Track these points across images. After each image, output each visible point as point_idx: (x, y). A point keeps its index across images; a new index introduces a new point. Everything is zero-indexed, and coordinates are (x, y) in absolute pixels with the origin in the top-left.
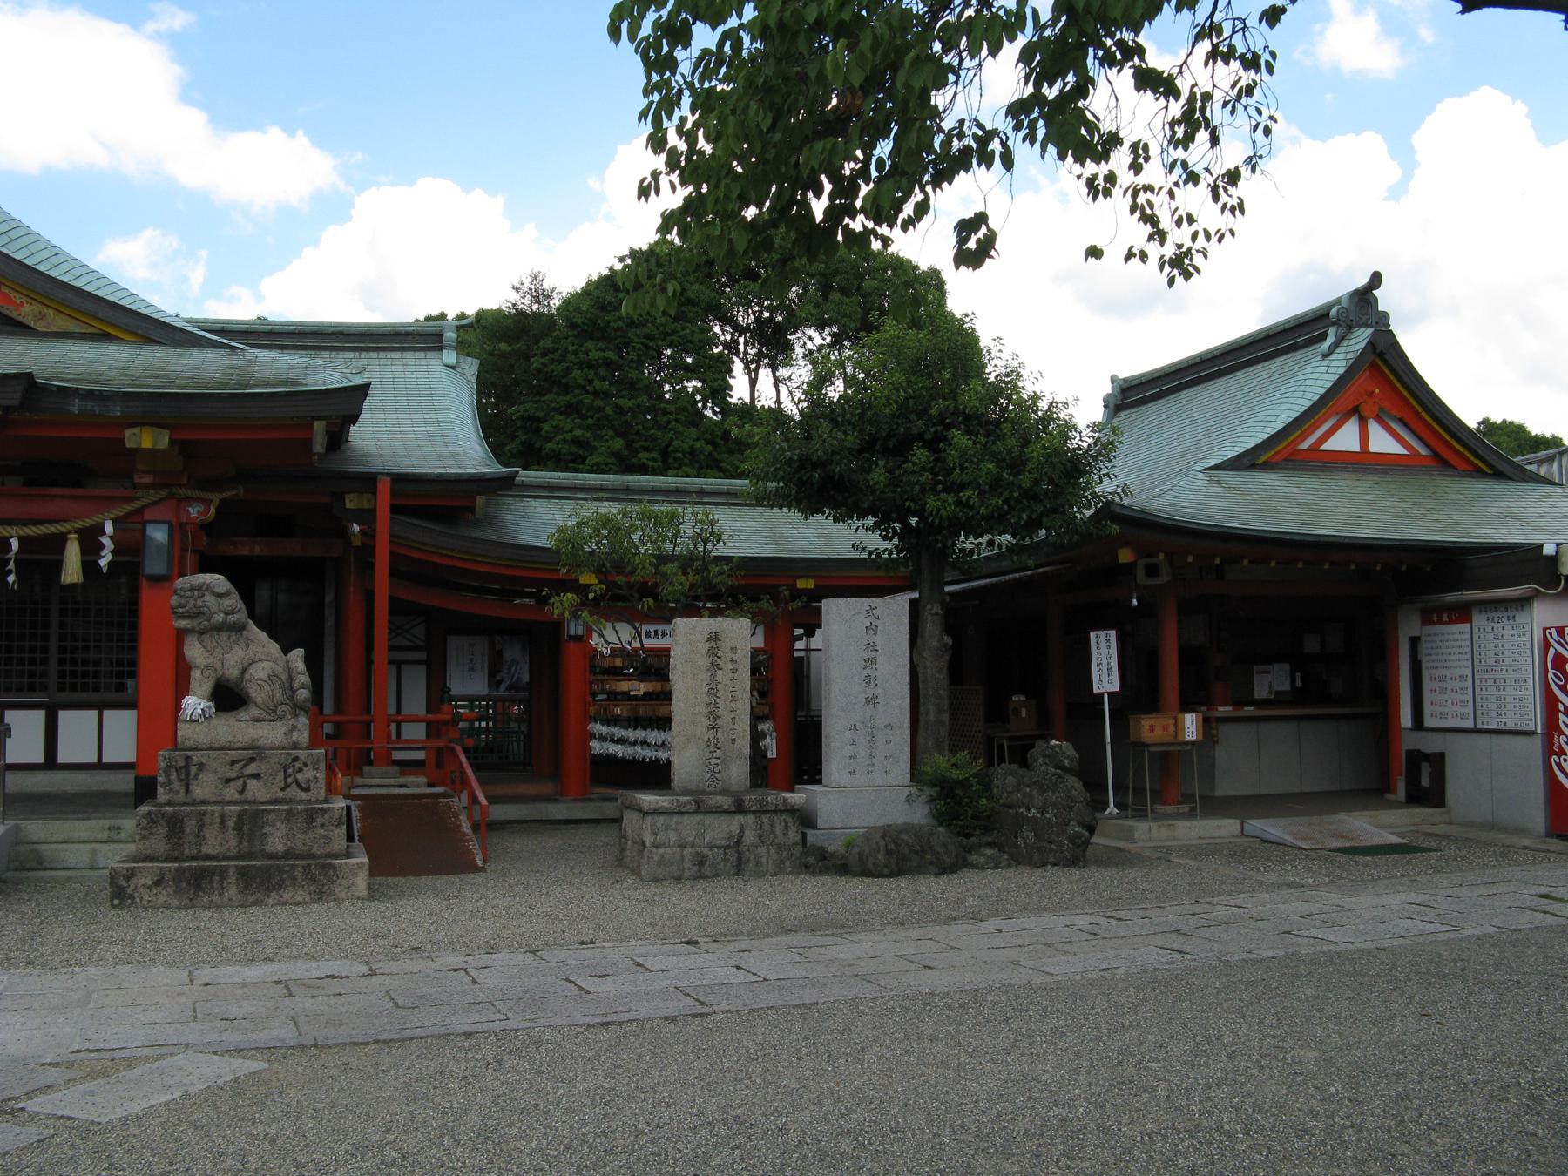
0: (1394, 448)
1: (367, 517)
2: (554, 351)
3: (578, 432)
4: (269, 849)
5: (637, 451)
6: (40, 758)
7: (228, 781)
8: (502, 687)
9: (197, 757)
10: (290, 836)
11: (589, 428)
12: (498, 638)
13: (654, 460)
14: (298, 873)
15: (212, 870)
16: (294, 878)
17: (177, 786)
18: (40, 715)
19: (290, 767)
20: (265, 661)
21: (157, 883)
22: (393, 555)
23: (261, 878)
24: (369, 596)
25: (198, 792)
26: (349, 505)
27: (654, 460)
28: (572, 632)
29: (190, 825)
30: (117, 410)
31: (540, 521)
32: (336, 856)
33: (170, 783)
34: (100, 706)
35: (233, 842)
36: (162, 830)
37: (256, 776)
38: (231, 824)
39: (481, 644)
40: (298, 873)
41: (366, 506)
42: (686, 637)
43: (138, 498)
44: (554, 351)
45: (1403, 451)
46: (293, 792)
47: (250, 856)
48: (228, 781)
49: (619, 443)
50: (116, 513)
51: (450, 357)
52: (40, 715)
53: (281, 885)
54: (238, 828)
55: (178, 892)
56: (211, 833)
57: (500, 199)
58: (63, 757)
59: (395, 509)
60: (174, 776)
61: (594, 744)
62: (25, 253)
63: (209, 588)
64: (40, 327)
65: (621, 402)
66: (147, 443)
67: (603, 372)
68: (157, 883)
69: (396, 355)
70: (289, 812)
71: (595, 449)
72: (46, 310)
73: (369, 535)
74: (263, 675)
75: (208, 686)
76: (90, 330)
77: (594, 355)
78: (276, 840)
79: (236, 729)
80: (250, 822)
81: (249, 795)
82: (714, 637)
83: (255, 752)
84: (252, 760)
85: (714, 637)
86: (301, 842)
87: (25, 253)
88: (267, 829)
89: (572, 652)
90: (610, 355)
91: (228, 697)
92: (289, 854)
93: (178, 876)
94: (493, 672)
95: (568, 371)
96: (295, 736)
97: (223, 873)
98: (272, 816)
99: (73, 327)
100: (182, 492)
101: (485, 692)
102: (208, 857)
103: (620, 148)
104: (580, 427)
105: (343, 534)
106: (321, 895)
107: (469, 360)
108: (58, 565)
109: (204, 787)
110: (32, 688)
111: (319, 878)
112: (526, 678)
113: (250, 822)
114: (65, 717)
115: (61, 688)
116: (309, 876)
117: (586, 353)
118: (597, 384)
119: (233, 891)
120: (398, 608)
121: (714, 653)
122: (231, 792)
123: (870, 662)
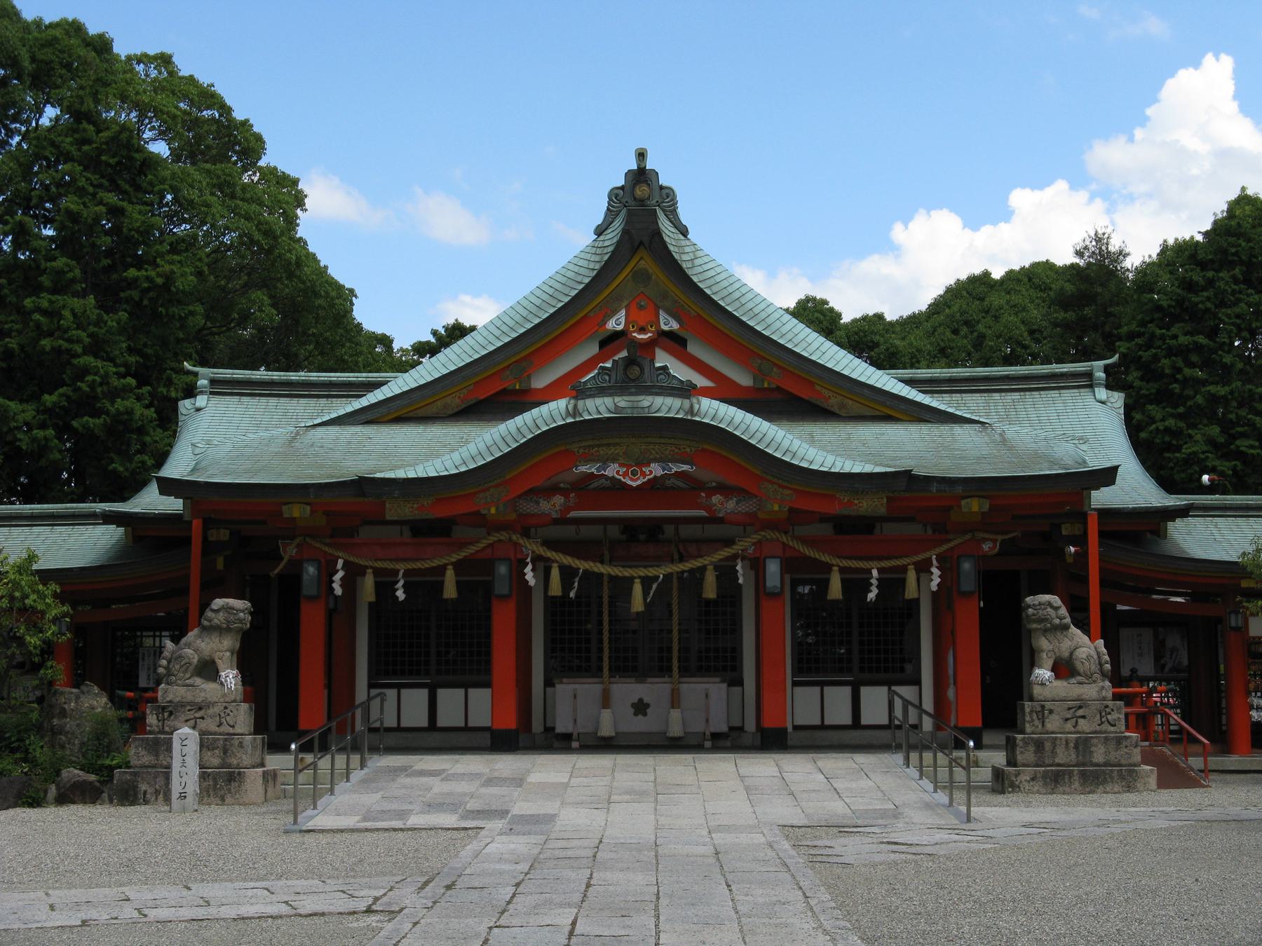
1: (1081, 540)
2: (1139, 335)
3: (1171, 422)
4: (1095, 760)
5: (1234, 437)
7: (1067, 720)
8: (1167, 669)
9: (1048, 705)
10: (1107, 753)
11: (1180, 417)
12: (1161, 629)
13: (1252, 447)
14: (1115, 774)
15: (1064, 772)
16: (1112, 778)
17: (1037, 722)
19: (1104, 711)
20: (1087, 648)
21: (1033, 779)
22: (1101, 570)
25: (1049, 726)
26: (1064, 533)
27: (1252, 447)
28: (1233, 624)
29: (1048, 745)
30: (959, 490)
32: (1135, 765)
33: (1033, 720)
34: (466, 686)
35: (1074, 756)
36: (1032, 748)
37: (1083, 717)
38: (1072, 745)
39: (1147, 634)
40: (1115, 774)
41: (1077, 533)
43: (950, 540)
44: (1139, 335)
46: (1105, 727)
47: (1084, 765)
48: (1067, 720)
49: (1215, 430)
50: (938, 550)
51: (1102, 393)
53: (1105, 782)
54: (1076, 747)
55: (1045, 784)
56: (1060, 750)
58: (865, 721)
59: (1102, 534)
60: (1035, 716)
61: (1254, 713)
62: (819, 353)
63: (1050, 604)
65: (1212, 389)
66: (975, 508)
67: (1194, 358)
68: (1033, 779)
69: (1054, 393)
70: (1106, 738)
71: (1190, 436)
72: (846, 401)
73: (1082, 556)
74: (1084, 656)
75: (1050, 663)
76: (878, 413)
77: (1183, 340)
78: (1099, 755)
79: (1062, 688)
80: (1083, 745)
81: (1079, 728)
83: (1081, 703)
84: (1080, 707)
86: (1114, 756)
87: (819, 353)
88: (1093, 749)
90: (1201, 339)
91: (1064, 669)
93: (1045, 776)
94: (1158, 658)
95: (1156, 358)
96: (1104, 693)
97: (1071, 774)
98: (1095, 741)
100: (980, 535)
101: (1152, 674)
102: (1059, 765)
104: (1172, 415)
105: (1062, 552)
106: (1129, 788)
107: (1116, 394)
109: (1053, 723)
110: (841, 671)
111: (1127, 779)
112: (1185, 662)
113: (1083, 745)
115: (862, 670)
116: (1122, 777)
117: (1175, 337)
118: (1187, 371)
119: (1077, 784)
122: (1069, 726)
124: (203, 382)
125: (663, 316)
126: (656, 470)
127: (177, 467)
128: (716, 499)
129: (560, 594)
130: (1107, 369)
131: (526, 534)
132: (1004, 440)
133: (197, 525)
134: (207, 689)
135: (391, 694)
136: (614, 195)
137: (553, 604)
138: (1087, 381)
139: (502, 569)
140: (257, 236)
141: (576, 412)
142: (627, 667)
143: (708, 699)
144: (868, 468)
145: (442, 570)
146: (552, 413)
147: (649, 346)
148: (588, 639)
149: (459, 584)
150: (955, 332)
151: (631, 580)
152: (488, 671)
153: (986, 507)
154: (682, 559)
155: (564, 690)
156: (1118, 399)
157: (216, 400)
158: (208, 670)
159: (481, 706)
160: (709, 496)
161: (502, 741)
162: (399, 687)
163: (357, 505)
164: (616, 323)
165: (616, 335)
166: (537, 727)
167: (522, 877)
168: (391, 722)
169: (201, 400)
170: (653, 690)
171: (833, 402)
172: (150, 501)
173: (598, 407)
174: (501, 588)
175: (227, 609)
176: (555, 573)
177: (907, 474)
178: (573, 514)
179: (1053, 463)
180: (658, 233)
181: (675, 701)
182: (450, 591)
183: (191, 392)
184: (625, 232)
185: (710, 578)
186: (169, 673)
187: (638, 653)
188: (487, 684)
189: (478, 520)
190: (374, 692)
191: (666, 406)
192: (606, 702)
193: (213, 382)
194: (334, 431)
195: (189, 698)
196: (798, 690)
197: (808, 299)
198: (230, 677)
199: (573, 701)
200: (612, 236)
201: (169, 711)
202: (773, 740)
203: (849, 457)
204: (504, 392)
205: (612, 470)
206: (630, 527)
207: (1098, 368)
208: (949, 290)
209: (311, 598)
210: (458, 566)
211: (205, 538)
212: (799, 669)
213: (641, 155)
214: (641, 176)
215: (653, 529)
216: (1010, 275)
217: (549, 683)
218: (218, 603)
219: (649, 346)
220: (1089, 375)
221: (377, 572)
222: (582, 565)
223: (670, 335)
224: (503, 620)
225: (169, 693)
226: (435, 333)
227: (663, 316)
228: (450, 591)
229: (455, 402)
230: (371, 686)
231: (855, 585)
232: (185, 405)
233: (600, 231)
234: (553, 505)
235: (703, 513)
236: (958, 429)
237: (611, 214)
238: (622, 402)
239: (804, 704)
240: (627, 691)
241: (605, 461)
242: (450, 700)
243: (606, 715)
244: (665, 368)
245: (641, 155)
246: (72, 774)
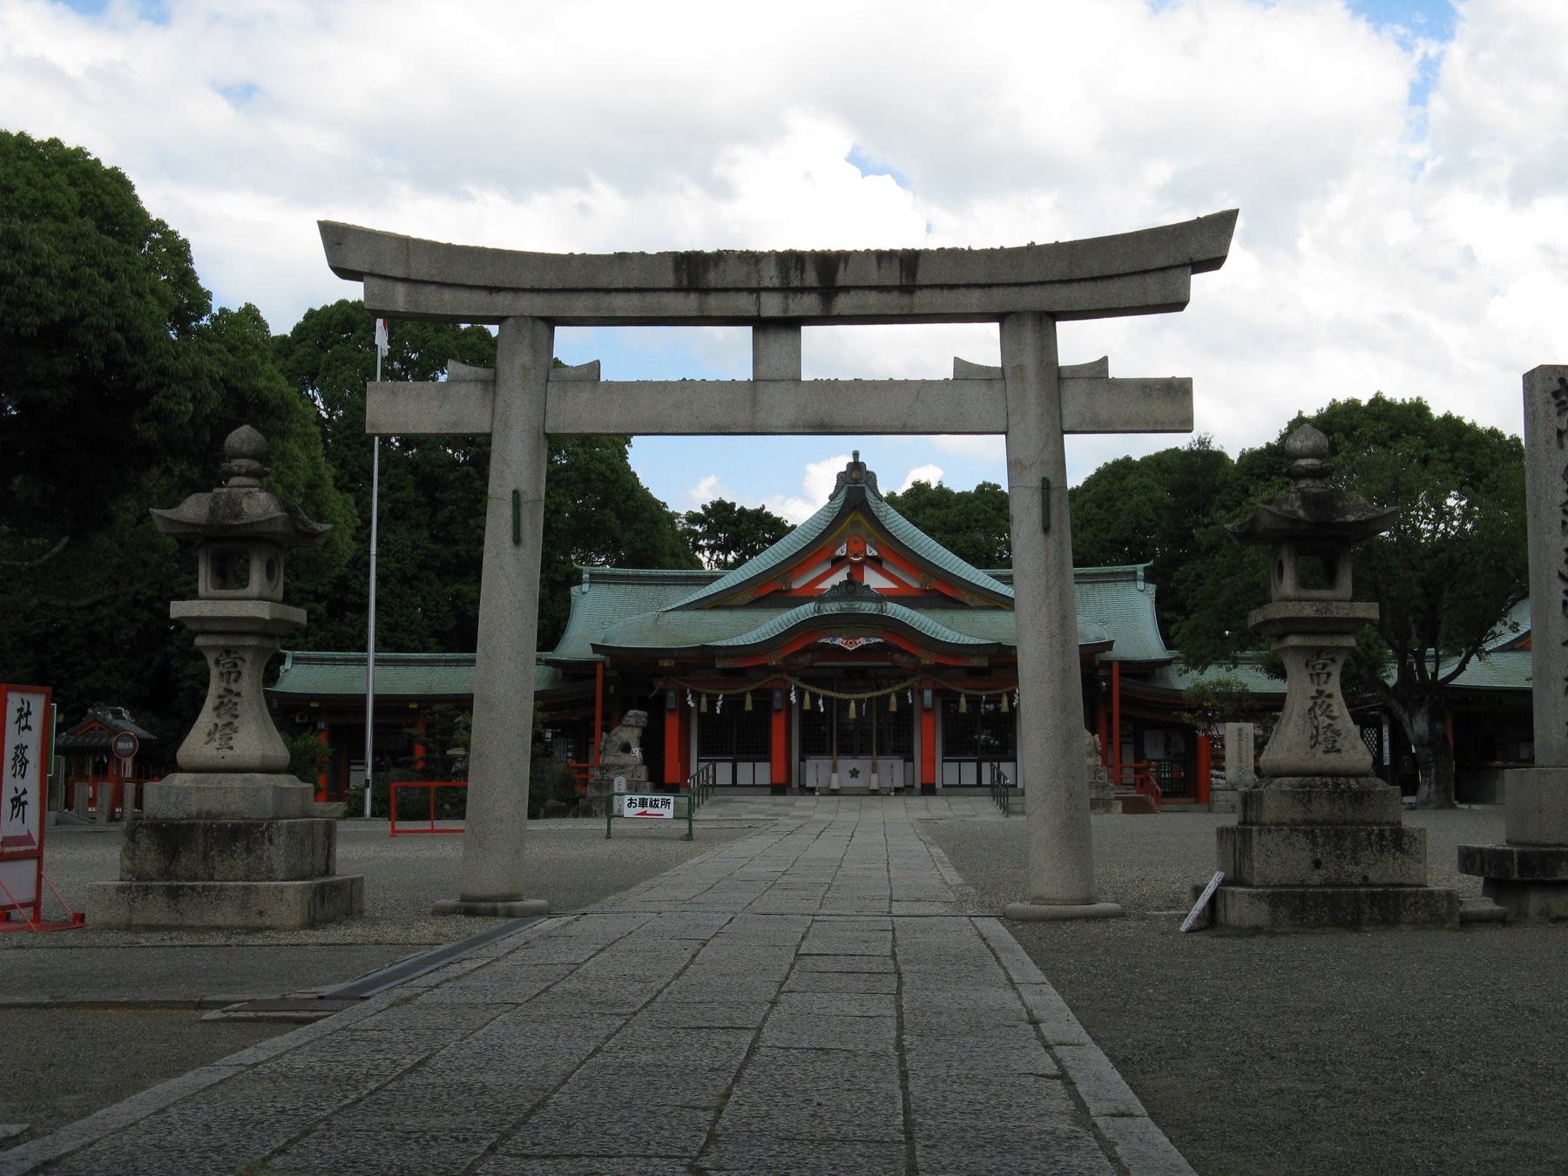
0: (886, 584)
1: (1109, 678)
18: (974, 765)
24: (1110, 718)
31: (1185, 681)
34: (754, 761)
42: (1230, 730)
45: (893, 586)
51: (1141, 585)
52: (974, 765)
57: (1234, 456)
58: (739, 782)
59: (1121, 675)
69: (1112, 585)
73: (1110, 687)
94: (1167, 747)
103: (1364, 403)
105: (1100, 687)
106: (1107, 811)
108: (743, 702)
114: (740, 765)
120: (1122, 717)
124: (586, 576)
125: (868, 548)
126: (863, 641)
128: (896, 656)
129: (172, 616)
131: (790, 674)
134: (626, 759)
136: (841, 476)
137: (804, 715)
138: (1132, 577)
139: (778, 695)
140: (608, 473)
142: (847, 750)
143: (893, 770)
144: (978, 641)
145: (744, 694)
146: (806, 611)
147: (861, 564)
148: (823, 736)
149: (754, 703)
150: (1099, 506)
151: (848, 702)
154: (878, 689)
155: (811, 763)
156: (1152, 588)
157: (594, 587)
158: (626, 748)
159: (763, 773)
161: (778, 789)
163: (699, 662)
164: (841, 551)
165: (840, 558)
166: (795, 784)
167: (722, 1082)
169: (585, 587)
170: (862, 764)
171: (967, 599)
174: (777, 705)
175: (636, 716)
176: (807, 696)
180: (865, 501)
181: (874, 770)
182: (749, 707)
183: (579, 582)
184: (846, 500)
185: (893, 699)
187: (852, 742)
188: (769, 760)
189: (766, 668)
191: (868, 608)
192: (834, 770)
193: (592, 575)
194: (679, 614)
197: (985, 485)
198: (636, 751)
199: (817, 771)
200: (839, 501)
202: (928, 790)
204: (777, 591)
205: (839, 641)
206: (849, 672)
207: (1140, 569)
208: (1099, 471)
209: (778, 711)
210: (754, 693)
212: (946, 752)
213: (856, 454)
215: (862, 672)
216: (1144, 460)
217: (802, 759)
218: (631, 712)
219: (861, 564)
220: (1134, 573)
221: (708, 696)
222: (822, 692)
223: (873, 558)
224: (777, 724)
226: (704, 507)
227: (868, 548)
228: (749, 707)
229: (748, 597)
231: (974, 702)
232: (574, 590)
233: (832, 498)
234: (804, 660)
238: (844, 605)
239: (948, 773)
240: (847, 764)
241: (835, 637)
242: (745, 770)
243: (835, 777)
245: (856, 454)
246: (551, 802)
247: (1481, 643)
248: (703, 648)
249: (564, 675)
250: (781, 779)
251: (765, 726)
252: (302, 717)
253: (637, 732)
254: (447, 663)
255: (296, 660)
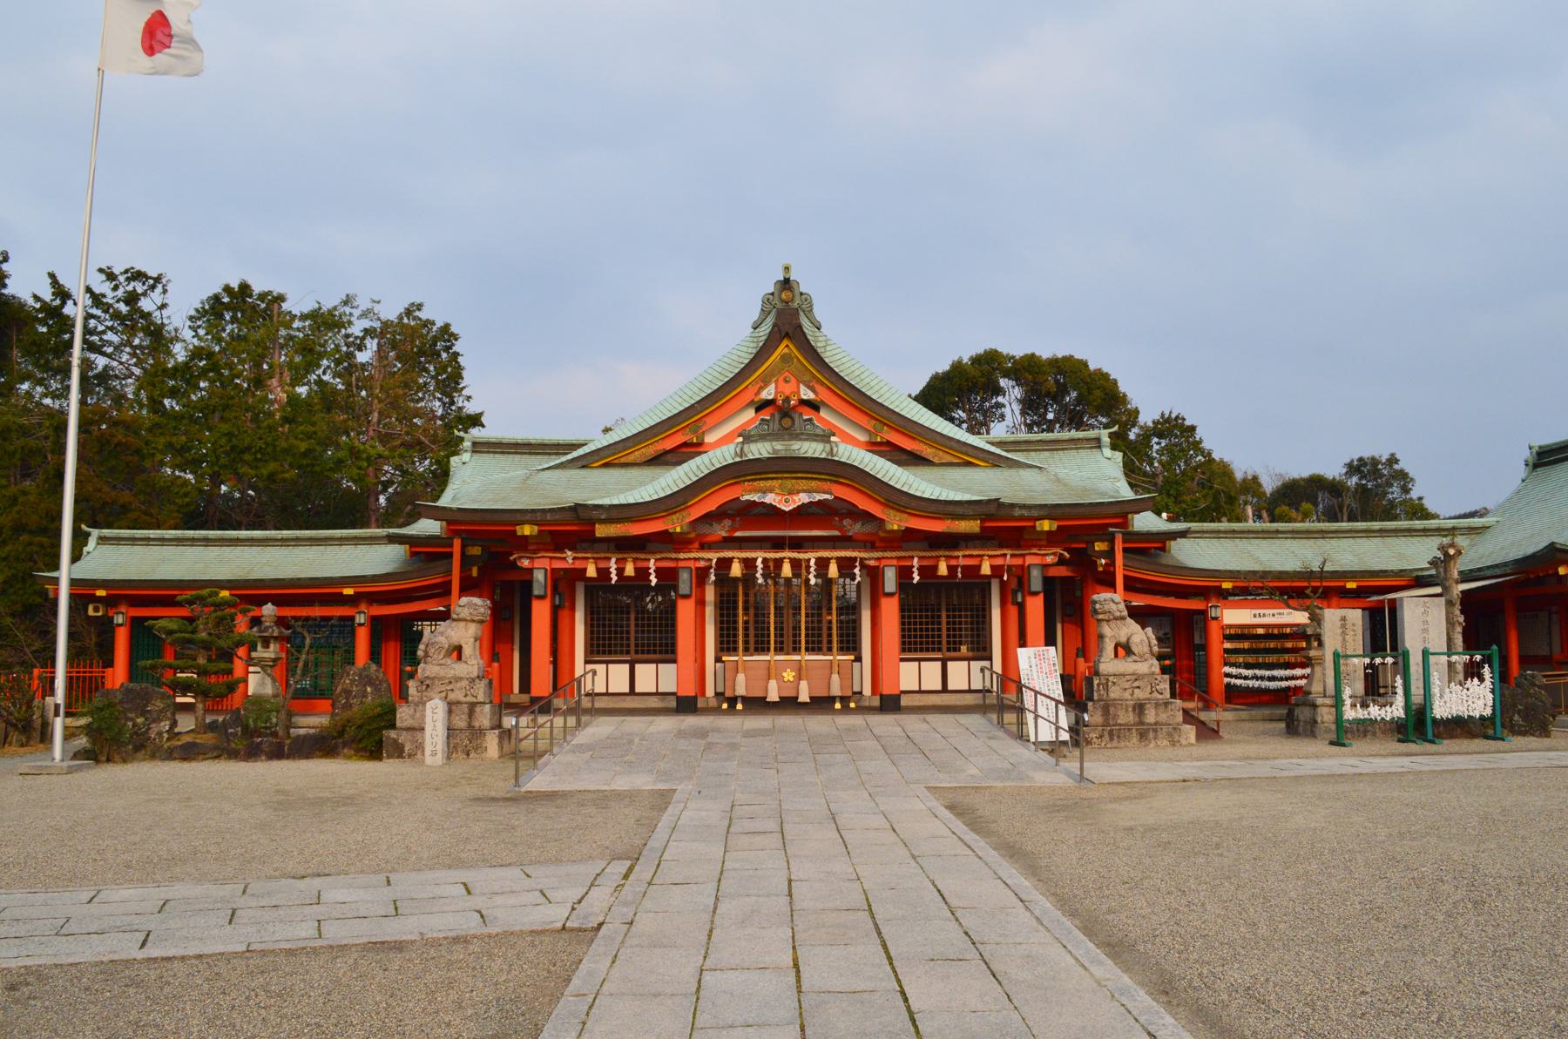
1: (1110, 554)
6: (627, 690)
18: (627, 666)
23: (1145, 733)
30: (1035, 513)
34: (657, 662)
42: (1332, 616)
46: (1156, 695)
51: (1107, 452)
52: (627, 666)
64: (936, 460)
66: (1046, 528)
69: (1073, 452)
80: (1140, 708)
82: (1344, 619)
85: (1344, 619)
89: (1214, 626)
92: (1156, 723)
99: (948, 458)
110: (621, 653)
113: (1140, 708)
115: (637, 652)
121: (1343, 626)
123: (1425, 631)
125: (803, 388)
126: (803, 498)
127: (444, 501)
128: (846, 522)
130: (1111, 435)
132: (1058, 480)
133: (457, 543)
134: (460, 669)
135: (600, 668)
136: (767, 300)
138: (1097, 444)
141: (742, 453)
144: (959, 497)
152: (674, 652)
153: (1054, 528)
156: (1119, 456)
157: (477, 456)
160: (841, 520)
162: (607, 662)
168: (600, 688)
169: (466, 457)
171: (927, 452)
172: (428, 527)
173: (760, 450)
175: (469, 605)
177: (996, 502)
178: (738, 534)
179: (1103, 494)
180: (800, 326)
184: (775, 325)
186: (427, 655)
190: (589, 667)
193: (475, 444)
195: (442, 673)
196: (902, 664)
200: (766, 329)
201: (426, 685)
203: (943, 486)
204: (685, 445)
205: (770, 499)
211: (463, 554)
213: (787, 269)
214: (786, 284)
220: (1098, 440)
225: (425, 670)
229: (650, 451)
230: (587, 662)
235: (836, 533)
236: (1024, 473)
237: (765, 313)
238: (778, 446)
241: (765, 492)
242: (645, 672)
244: (810, 420)
245: (787, 269)
247: (414, 653)
248: (577, 508)
249: (413, 554)
250: (689, 690)
251: (669, 613)
252: (96, 609)
253: (473, 629)
254: (284, 542)
255: (102, 540)
